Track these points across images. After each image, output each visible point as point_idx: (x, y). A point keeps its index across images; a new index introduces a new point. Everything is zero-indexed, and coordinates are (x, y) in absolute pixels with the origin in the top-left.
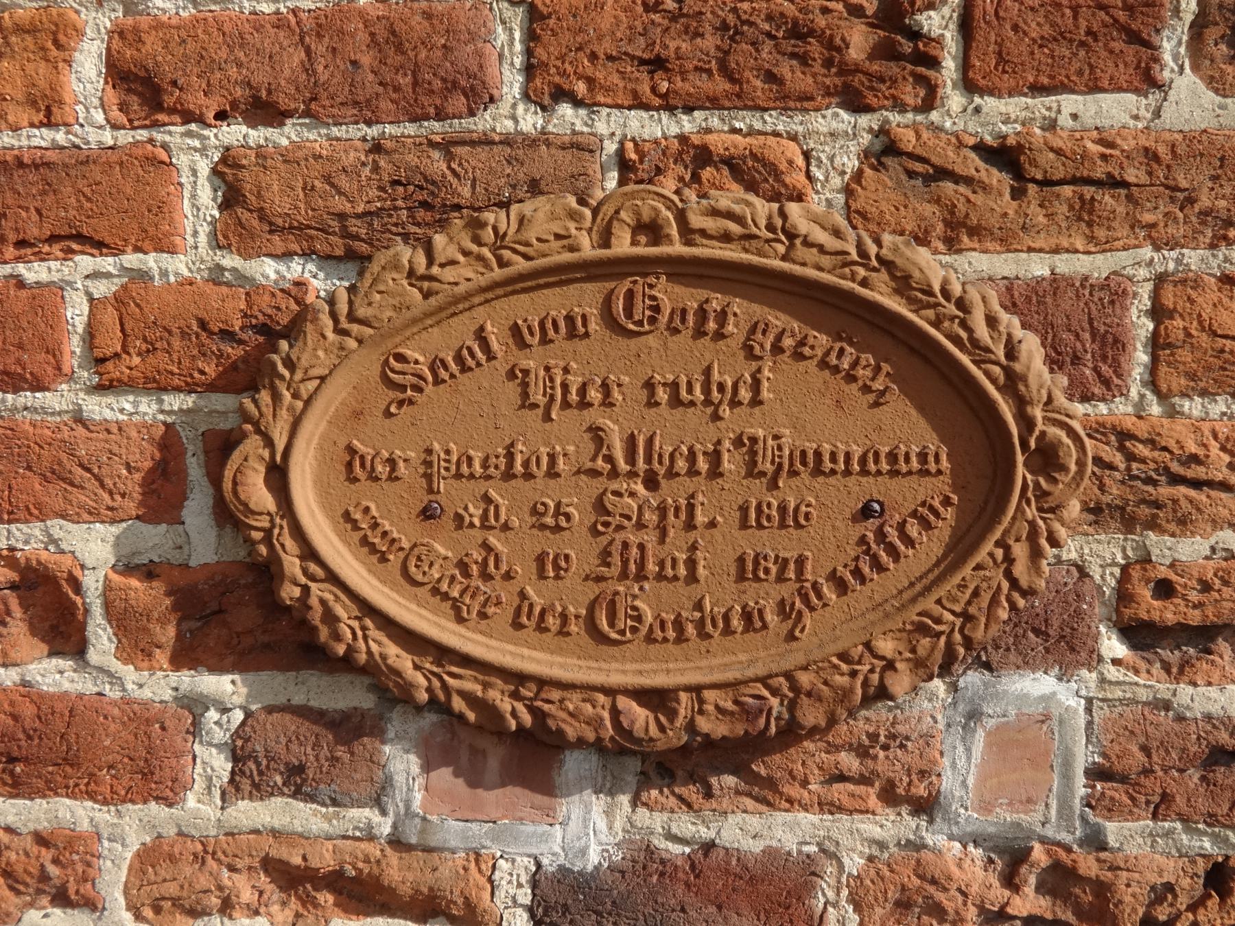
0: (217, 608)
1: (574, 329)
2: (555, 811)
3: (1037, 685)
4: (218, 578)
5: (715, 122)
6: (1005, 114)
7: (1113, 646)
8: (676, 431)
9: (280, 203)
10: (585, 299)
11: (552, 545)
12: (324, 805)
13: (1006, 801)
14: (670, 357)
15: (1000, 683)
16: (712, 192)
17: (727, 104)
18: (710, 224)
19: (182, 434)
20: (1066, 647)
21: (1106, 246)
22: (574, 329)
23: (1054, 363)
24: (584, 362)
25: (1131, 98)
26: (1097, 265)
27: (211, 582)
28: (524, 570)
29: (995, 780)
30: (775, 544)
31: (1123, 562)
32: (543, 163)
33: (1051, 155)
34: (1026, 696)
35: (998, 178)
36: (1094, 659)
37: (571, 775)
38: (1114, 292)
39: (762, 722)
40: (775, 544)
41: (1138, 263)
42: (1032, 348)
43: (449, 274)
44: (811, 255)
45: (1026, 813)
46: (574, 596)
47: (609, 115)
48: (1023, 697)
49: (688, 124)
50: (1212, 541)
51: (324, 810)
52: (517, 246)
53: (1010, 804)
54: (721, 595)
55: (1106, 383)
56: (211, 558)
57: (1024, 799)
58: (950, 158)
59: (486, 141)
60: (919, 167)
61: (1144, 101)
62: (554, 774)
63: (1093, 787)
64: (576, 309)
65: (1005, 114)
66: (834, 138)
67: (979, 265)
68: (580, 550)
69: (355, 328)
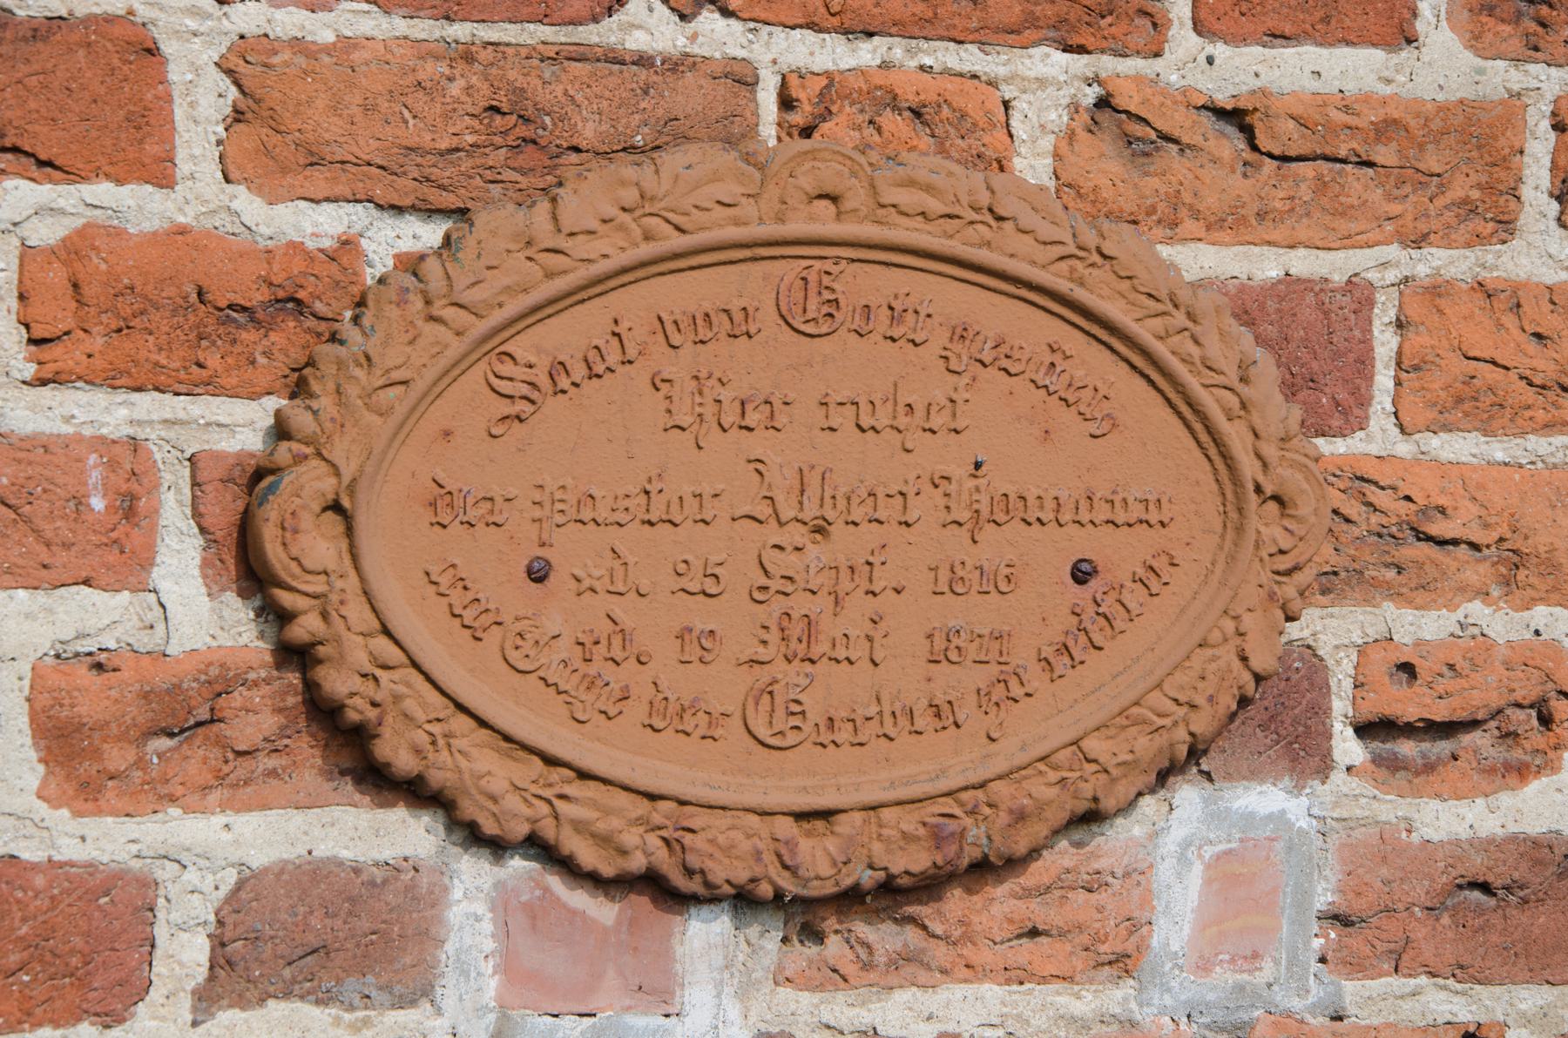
0: (207, 716)
1: (740, 325)
2: (673, 994)
3: (1266, 799)
4: (214, 671)
5: (898, 53)
6: (1241, 69)
7: (1348, 748)
8: (858, 462)
9: (325, 126)
10: (750, 285)
11: (701, 616)
12: (351, 1008)
13: (1227, 957)
14: (852, 364)
15: (1222, 798)
16: (904, 156)
17: (916, 31)
18: (903, 197)
19: (158, 456)
20: (1304, 754)
21: (1348, 241)
22: (740, 325)
23: (1290, 390)
24: (749, 367)
25: (1378, 55)
26: (1334, 265)
27: (203, 677)
28: (664, 652)
29: (1215, 929)
30: (976, 613)
31: (1360, 642)
32: (688, 97)
33: (1291, 124)
34: (1252, 815)
35: (1231, 144)
36: (1324, 767)
37: (697, 944)
38: (1359, 294)
39: (954, 848)
40: (976, 613)
41: (1383, 264)
42: (1267, 371)
43: (580, 247)
44: (1025, 244)
45: (1250, 972)
46: (724, 686)
47: (770, 34)
48: (1249, 818)
49: (867, 54)
50: (1460, 614)
51: (347, 1016)
52: (670, 216)
53: (1232, 961)
54: (907, 679)
55: (1345, 413)
56: (201, 642)
57: (1249, 953)
58: (1176, 121)
59: (615, 58)
60: (1138, 129)
61: (1388, 110)
62: (675, 941)
63: (1327, 937)
64: (735, 301)
65: (1241, 69)
66: (1042, 87)
67: (1199, 260)
68: (737, 623)
69: (449, 313)
